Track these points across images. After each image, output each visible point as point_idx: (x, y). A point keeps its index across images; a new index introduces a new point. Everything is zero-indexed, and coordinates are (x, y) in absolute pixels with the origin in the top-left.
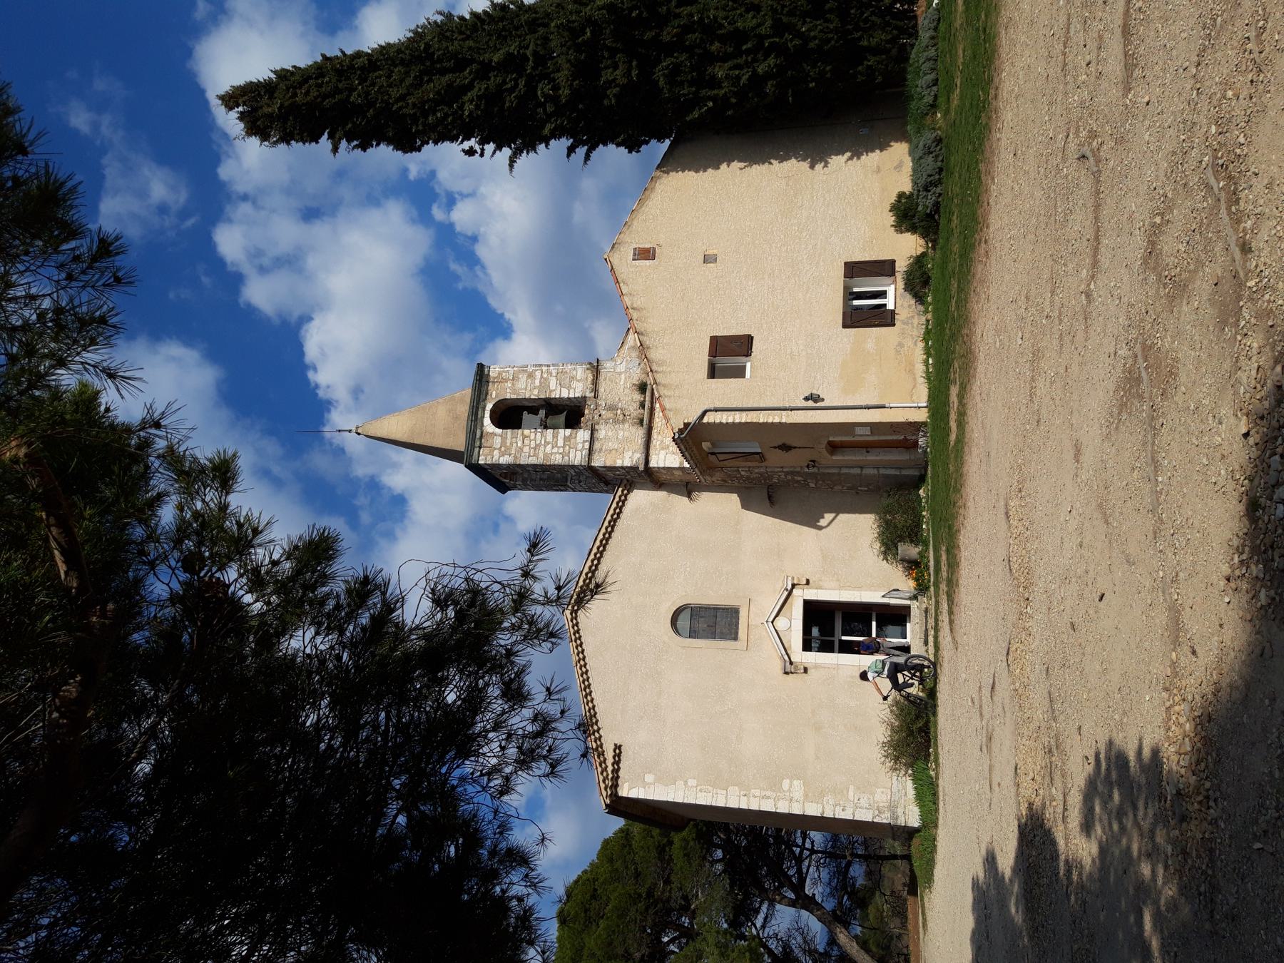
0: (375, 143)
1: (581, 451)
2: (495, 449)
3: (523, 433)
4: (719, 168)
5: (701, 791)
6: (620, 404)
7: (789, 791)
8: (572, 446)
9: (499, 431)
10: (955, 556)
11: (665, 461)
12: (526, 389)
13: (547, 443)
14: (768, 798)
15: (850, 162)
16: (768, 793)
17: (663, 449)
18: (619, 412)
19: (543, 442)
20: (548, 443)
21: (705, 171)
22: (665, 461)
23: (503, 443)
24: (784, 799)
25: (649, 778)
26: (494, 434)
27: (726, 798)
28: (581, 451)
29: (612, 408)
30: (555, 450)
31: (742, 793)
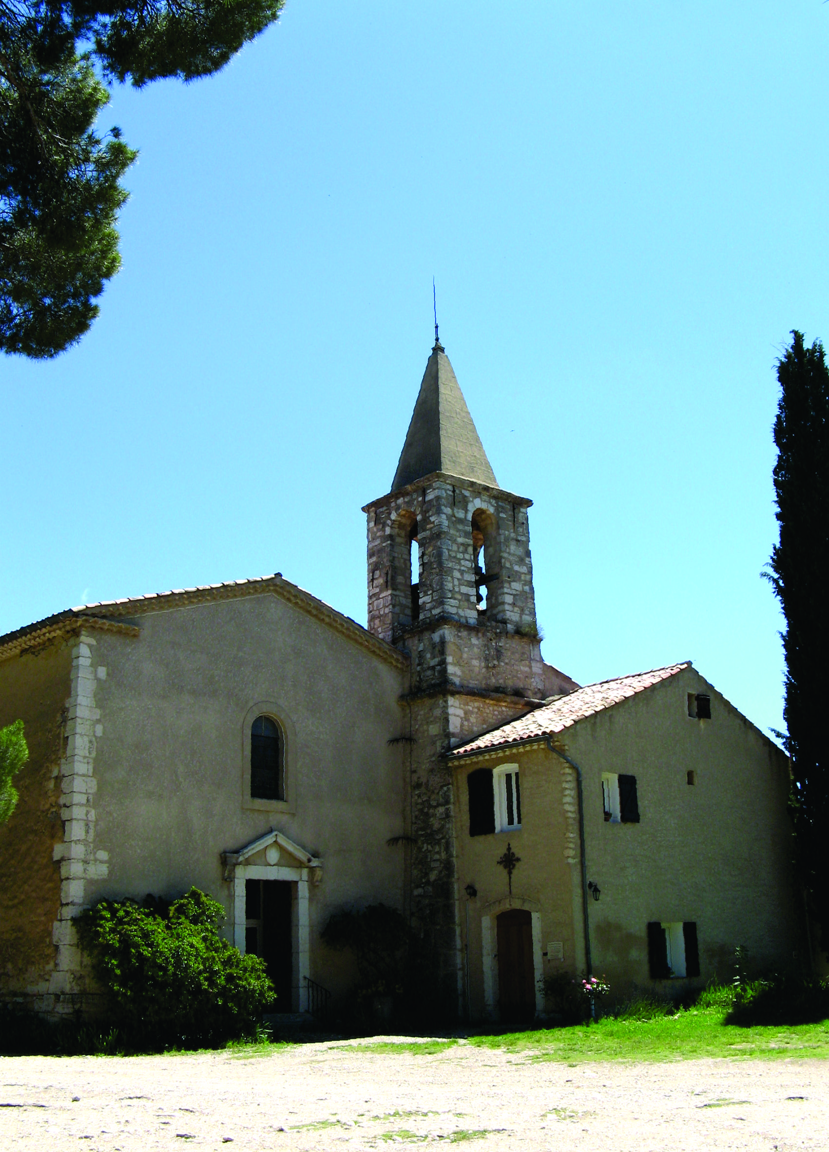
0: (775, 557)
1: (457, 613)
2: (453, 510)
3: (469, 545)
4: (778, 520)
5: (91, 742)
6: (502, 664)
7: (96, 860)
8: (461, 603)
9: (470, 517)
10: (582, 814)
11: (455, 715)
12: (509, 553)
13: (462, 572)
14: (87, 832)
15: (773, 546)
16: (92, 832)
17: (466, 713)
18: (496, 662)
19: (462, 568)
20: (462, 574)
21: (779, 517)
22: (455, 715)
23: (461, 521)
24: (86, 854)
25: (102, 672)
26: (466, 511)
27: (83, 775)
28: (457, 613)
29: (499, 654)
30: (456, 582)
31: (91, 797)
